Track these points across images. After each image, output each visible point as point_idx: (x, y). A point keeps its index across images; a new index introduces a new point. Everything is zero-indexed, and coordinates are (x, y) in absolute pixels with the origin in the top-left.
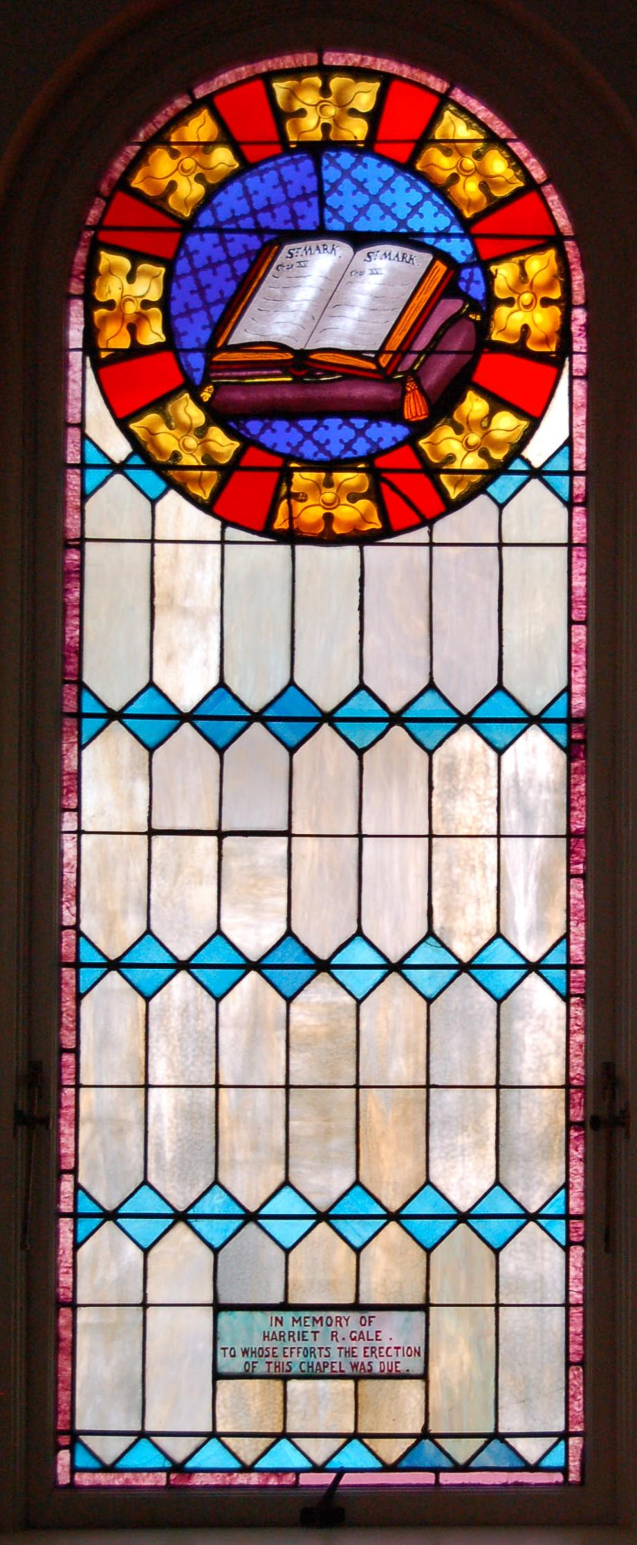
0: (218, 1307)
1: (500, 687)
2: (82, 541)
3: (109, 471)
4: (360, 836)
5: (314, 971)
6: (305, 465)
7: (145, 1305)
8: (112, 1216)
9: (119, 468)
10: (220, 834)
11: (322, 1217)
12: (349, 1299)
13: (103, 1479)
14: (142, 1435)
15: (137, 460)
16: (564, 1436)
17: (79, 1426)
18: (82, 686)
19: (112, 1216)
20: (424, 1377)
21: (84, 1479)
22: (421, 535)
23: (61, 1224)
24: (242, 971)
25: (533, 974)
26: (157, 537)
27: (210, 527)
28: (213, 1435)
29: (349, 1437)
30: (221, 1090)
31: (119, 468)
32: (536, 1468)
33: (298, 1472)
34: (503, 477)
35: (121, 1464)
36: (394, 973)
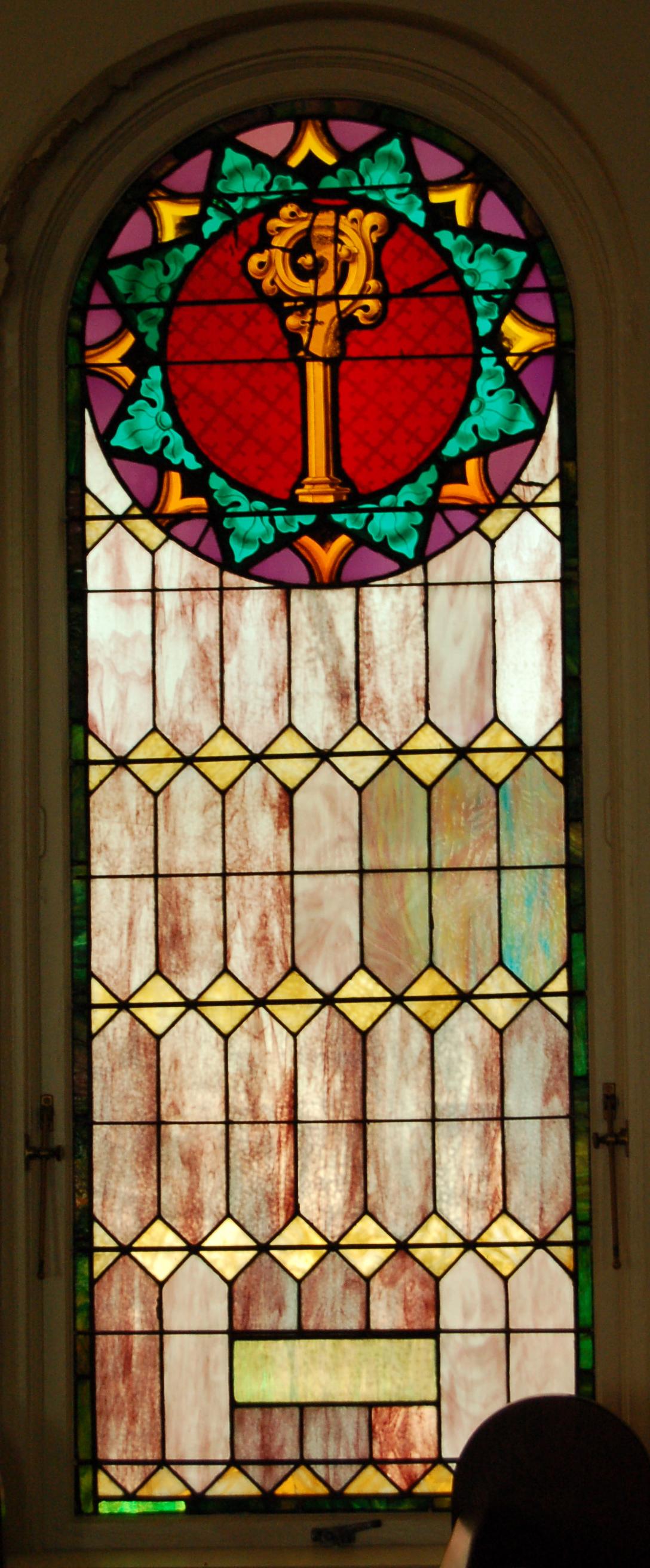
15: (136, 511)
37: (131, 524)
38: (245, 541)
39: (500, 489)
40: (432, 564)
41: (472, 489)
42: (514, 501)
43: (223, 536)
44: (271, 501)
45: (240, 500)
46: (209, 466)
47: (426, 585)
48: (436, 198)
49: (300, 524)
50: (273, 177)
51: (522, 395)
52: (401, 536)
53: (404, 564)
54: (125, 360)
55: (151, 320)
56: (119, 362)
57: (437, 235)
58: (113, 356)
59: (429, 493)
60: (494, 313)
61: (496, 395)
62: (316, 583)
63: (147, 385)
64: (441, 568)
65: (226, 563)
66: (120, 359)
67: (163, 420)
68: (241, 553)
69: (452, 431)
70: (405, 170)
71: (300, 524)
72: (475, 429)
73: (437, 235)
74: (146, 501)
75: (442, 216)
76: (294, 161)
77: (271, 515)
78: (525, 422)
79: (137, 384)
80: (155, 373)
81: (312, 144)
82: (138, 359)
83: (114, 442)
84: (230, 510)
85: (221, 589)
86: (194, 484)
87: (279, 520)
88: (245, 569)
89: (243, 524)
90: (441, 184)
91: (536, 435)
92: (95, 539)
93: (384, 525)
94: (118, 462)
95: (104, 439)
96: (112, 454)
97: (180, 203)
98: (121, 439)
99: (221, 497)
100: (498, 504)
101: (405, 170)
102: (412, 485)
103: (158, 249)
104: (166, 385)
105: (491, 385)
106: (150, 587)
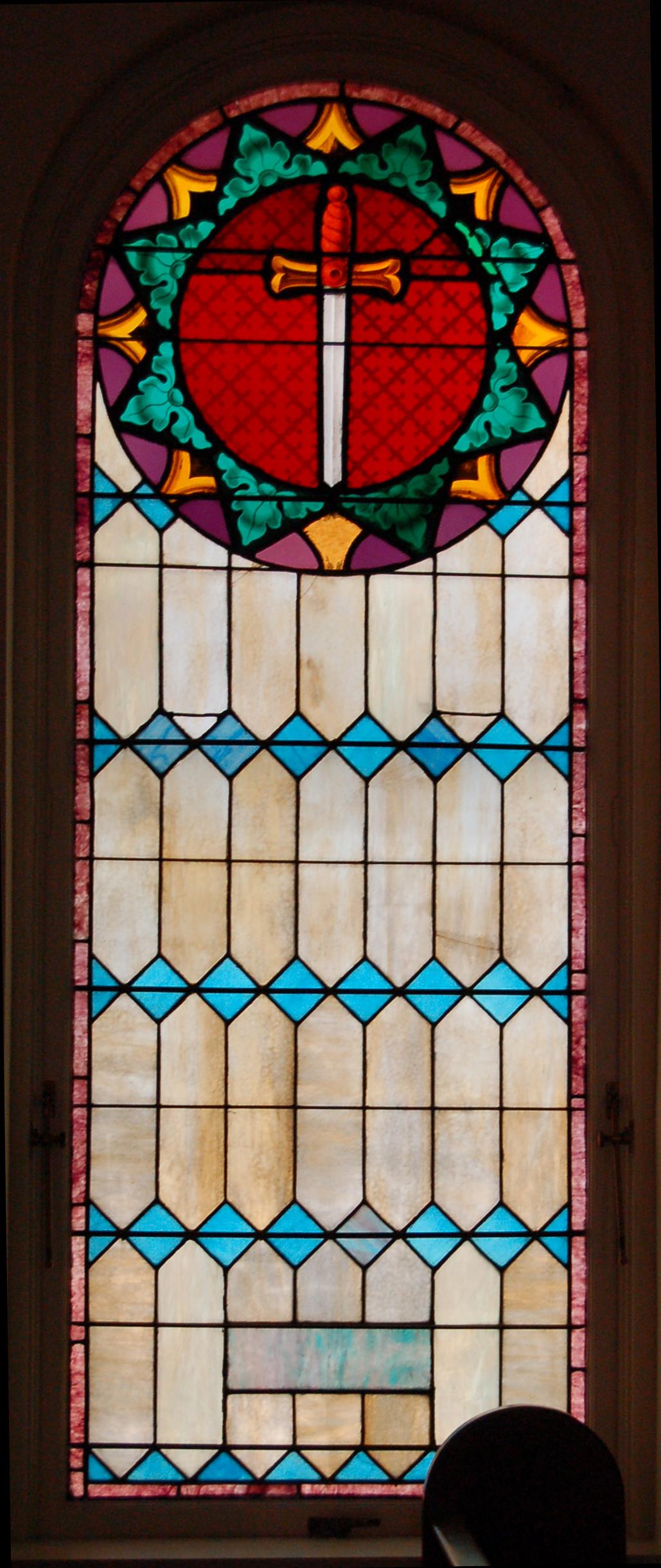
1: (367, 713)
2: (572, 577)
6: (302, 494)
9: (131, 497)
10: (296, 862)
12: (356, 1317)
13: (323, 1489)
14: (154, 1447)
15: (146, 490)
17: (93, 1439)
18: (93, 714)
21: (96, 1491)
22: (426, 565)
23: (73, 1243)
24: (456, 997)
26: (499, 572)
28: (294, 1448)
29: (357, 1449)
30: (437, 1112)
31: (131, 497)
32: (124, 1480)
34: (505, 507)
35: (341, 1476)
36: (397, 998)
38: (253, 523)
39: (509, 484)
41: (482, 486)
42: (524, 498)
43: (231, 518)
44: (280, 485)
45: (247, 482)
46: (219, 445)
47: (435, 574)
49: (308, 510)
51: (535, 396)
54: (136, 335)
55: (162, 298)
56: (129, 336)
58: (122, 330)
59: (184, 441)
61: (387, 160)
62: (321, 571)
64: (448, 559)
65: (233, 545)
66: (130, 334)
67: (174, 395)
68: (248, 535)
69: (464, 428)
71: (308, 510)
72: (488, 426)
74: (156, 478)
77: (280, 501)
78: (536, 421)
79: (148, 359)
80: (166, 349)
82: (150, 335)
83: (124, 418)
84: (238, 493)
86: (204, 463)
87: (287, 505)
88: (249, 552)
89: (250, 507)
91: (544, 436)
94: (127, 438)
95: (114, 412)
96: (121, 429)
98: (130, 415)
99: (230, 478)
100: (506, 500)
103: (173, 225)
104: (177, 361)
106: (157, 563)
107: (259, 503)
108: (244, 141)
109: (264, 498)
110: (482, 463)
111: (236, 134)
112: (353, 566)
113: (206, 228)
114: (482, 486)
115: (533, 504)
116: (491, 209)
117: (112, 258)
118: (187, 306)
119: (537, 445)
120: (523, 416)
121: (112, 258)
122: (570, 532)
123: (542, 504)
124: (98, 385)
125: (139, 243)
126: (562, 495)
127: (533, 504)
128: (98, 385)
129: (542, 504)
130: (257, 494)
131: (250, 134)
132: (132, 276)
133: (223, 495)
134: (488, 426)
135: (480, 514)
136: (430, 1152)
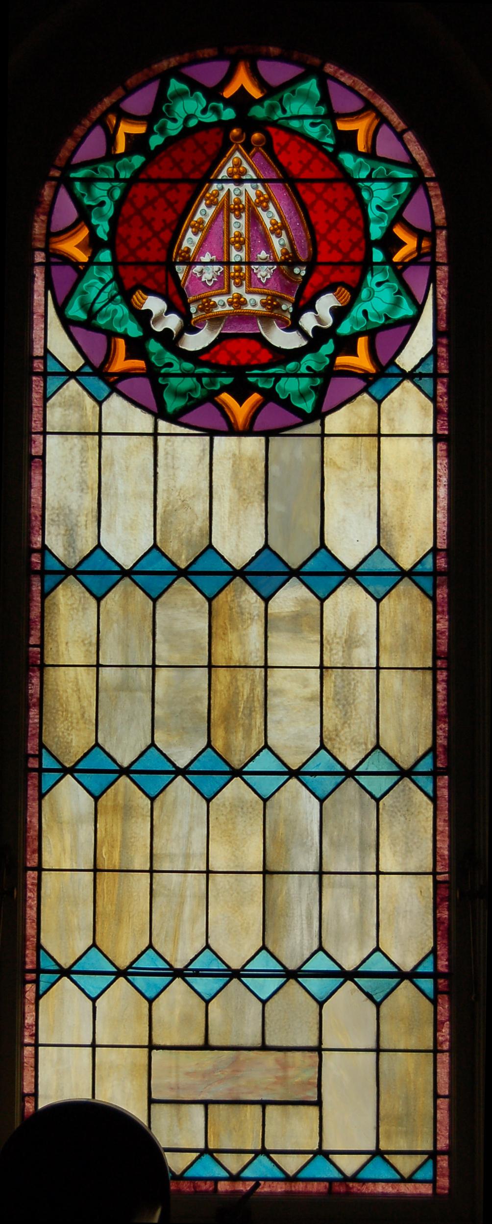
0: (319, 1049)
3: (66, 378)
4: (154, 666)
5: (399, 777)
7: (94, 1046)
8: (66, 972)
11: (120, 973)
15: (88, 369)
16: (433, 1155)
19: (66, 972)
20: (319, 1103)
22: (314, 427)
25: (69, 776)
27: (143, 421)
29: (257, 1153)
33: (216, 1180)
37: (83, 379)
39: (384, 361)
40: (328, 419)
43: (158, 391)
47: (323, 435)
48: (342, 126)
50: (208, 103)
51: (406, 289)
52: (303, 396)
53: (306, 418)
57: (152, 148)
60: (124, 162)
61: (382, 287)
62: (232, 431)
63: (235, 612)
64: (335, 422)
65: (160, 413)
68: (172, 404)
70: (320, 104)
72: (365, 313)
73: (152, 148)
75: (136, 144)
76: (228, 93)
77: (199, 377)
78: (406, 310)
81: (242, 80)
84: (163, 371)
85: (155, 434)
87: (205, 380)
88: (174, 418)
90: (111, 140)
91: (412, 322)
92: (53, 963)
93: (289, 386)
94: (73, 329)
96: (67, 323)
97: (127, 122)
101: (320, 104)
102: (313, 354)
105: (379, 278)
107: (181, 379)
108: (171, 90)
109: (184, 375)
110: (362, 343)
111: (164, 86)
112: (256, 428)
113: (138, 161)
114: (362, 361)
115: (405, 375)
116: (226, 410)
117: (62, 185)
118: (127, 209)
119: (407, 328)
120: (397, 304)
121: (62, 185)
122: (434, 399)
123: (411, 376)
124: (49, 292)
125: (81, 174)
126: (428, 368)
127: (405, 375)
128: (49, 292)
129: (411, 376)
130: (179, 372)
131: (175, 85)
132: (77, 201)
133: (152, 373)
134: (365, 313)
135: (362, 384)
136: (266, 927)
